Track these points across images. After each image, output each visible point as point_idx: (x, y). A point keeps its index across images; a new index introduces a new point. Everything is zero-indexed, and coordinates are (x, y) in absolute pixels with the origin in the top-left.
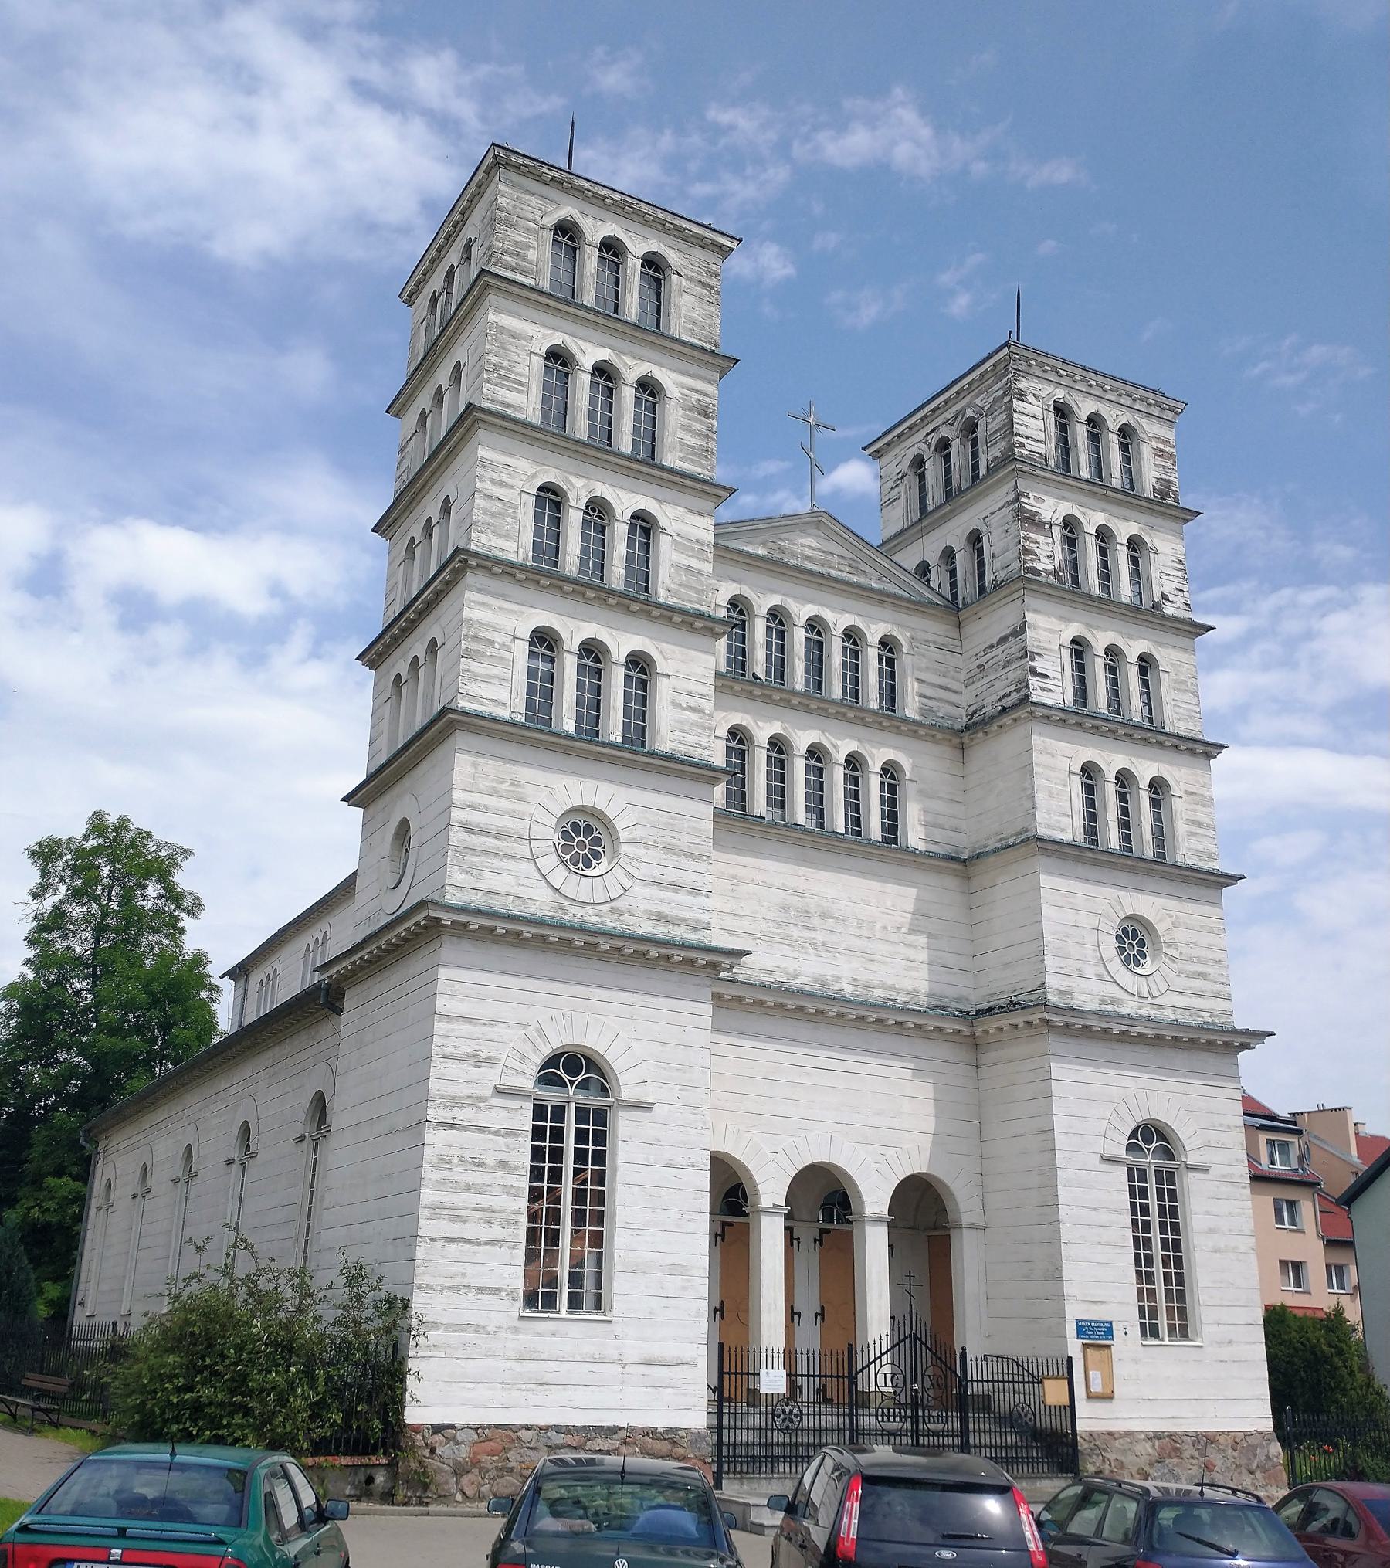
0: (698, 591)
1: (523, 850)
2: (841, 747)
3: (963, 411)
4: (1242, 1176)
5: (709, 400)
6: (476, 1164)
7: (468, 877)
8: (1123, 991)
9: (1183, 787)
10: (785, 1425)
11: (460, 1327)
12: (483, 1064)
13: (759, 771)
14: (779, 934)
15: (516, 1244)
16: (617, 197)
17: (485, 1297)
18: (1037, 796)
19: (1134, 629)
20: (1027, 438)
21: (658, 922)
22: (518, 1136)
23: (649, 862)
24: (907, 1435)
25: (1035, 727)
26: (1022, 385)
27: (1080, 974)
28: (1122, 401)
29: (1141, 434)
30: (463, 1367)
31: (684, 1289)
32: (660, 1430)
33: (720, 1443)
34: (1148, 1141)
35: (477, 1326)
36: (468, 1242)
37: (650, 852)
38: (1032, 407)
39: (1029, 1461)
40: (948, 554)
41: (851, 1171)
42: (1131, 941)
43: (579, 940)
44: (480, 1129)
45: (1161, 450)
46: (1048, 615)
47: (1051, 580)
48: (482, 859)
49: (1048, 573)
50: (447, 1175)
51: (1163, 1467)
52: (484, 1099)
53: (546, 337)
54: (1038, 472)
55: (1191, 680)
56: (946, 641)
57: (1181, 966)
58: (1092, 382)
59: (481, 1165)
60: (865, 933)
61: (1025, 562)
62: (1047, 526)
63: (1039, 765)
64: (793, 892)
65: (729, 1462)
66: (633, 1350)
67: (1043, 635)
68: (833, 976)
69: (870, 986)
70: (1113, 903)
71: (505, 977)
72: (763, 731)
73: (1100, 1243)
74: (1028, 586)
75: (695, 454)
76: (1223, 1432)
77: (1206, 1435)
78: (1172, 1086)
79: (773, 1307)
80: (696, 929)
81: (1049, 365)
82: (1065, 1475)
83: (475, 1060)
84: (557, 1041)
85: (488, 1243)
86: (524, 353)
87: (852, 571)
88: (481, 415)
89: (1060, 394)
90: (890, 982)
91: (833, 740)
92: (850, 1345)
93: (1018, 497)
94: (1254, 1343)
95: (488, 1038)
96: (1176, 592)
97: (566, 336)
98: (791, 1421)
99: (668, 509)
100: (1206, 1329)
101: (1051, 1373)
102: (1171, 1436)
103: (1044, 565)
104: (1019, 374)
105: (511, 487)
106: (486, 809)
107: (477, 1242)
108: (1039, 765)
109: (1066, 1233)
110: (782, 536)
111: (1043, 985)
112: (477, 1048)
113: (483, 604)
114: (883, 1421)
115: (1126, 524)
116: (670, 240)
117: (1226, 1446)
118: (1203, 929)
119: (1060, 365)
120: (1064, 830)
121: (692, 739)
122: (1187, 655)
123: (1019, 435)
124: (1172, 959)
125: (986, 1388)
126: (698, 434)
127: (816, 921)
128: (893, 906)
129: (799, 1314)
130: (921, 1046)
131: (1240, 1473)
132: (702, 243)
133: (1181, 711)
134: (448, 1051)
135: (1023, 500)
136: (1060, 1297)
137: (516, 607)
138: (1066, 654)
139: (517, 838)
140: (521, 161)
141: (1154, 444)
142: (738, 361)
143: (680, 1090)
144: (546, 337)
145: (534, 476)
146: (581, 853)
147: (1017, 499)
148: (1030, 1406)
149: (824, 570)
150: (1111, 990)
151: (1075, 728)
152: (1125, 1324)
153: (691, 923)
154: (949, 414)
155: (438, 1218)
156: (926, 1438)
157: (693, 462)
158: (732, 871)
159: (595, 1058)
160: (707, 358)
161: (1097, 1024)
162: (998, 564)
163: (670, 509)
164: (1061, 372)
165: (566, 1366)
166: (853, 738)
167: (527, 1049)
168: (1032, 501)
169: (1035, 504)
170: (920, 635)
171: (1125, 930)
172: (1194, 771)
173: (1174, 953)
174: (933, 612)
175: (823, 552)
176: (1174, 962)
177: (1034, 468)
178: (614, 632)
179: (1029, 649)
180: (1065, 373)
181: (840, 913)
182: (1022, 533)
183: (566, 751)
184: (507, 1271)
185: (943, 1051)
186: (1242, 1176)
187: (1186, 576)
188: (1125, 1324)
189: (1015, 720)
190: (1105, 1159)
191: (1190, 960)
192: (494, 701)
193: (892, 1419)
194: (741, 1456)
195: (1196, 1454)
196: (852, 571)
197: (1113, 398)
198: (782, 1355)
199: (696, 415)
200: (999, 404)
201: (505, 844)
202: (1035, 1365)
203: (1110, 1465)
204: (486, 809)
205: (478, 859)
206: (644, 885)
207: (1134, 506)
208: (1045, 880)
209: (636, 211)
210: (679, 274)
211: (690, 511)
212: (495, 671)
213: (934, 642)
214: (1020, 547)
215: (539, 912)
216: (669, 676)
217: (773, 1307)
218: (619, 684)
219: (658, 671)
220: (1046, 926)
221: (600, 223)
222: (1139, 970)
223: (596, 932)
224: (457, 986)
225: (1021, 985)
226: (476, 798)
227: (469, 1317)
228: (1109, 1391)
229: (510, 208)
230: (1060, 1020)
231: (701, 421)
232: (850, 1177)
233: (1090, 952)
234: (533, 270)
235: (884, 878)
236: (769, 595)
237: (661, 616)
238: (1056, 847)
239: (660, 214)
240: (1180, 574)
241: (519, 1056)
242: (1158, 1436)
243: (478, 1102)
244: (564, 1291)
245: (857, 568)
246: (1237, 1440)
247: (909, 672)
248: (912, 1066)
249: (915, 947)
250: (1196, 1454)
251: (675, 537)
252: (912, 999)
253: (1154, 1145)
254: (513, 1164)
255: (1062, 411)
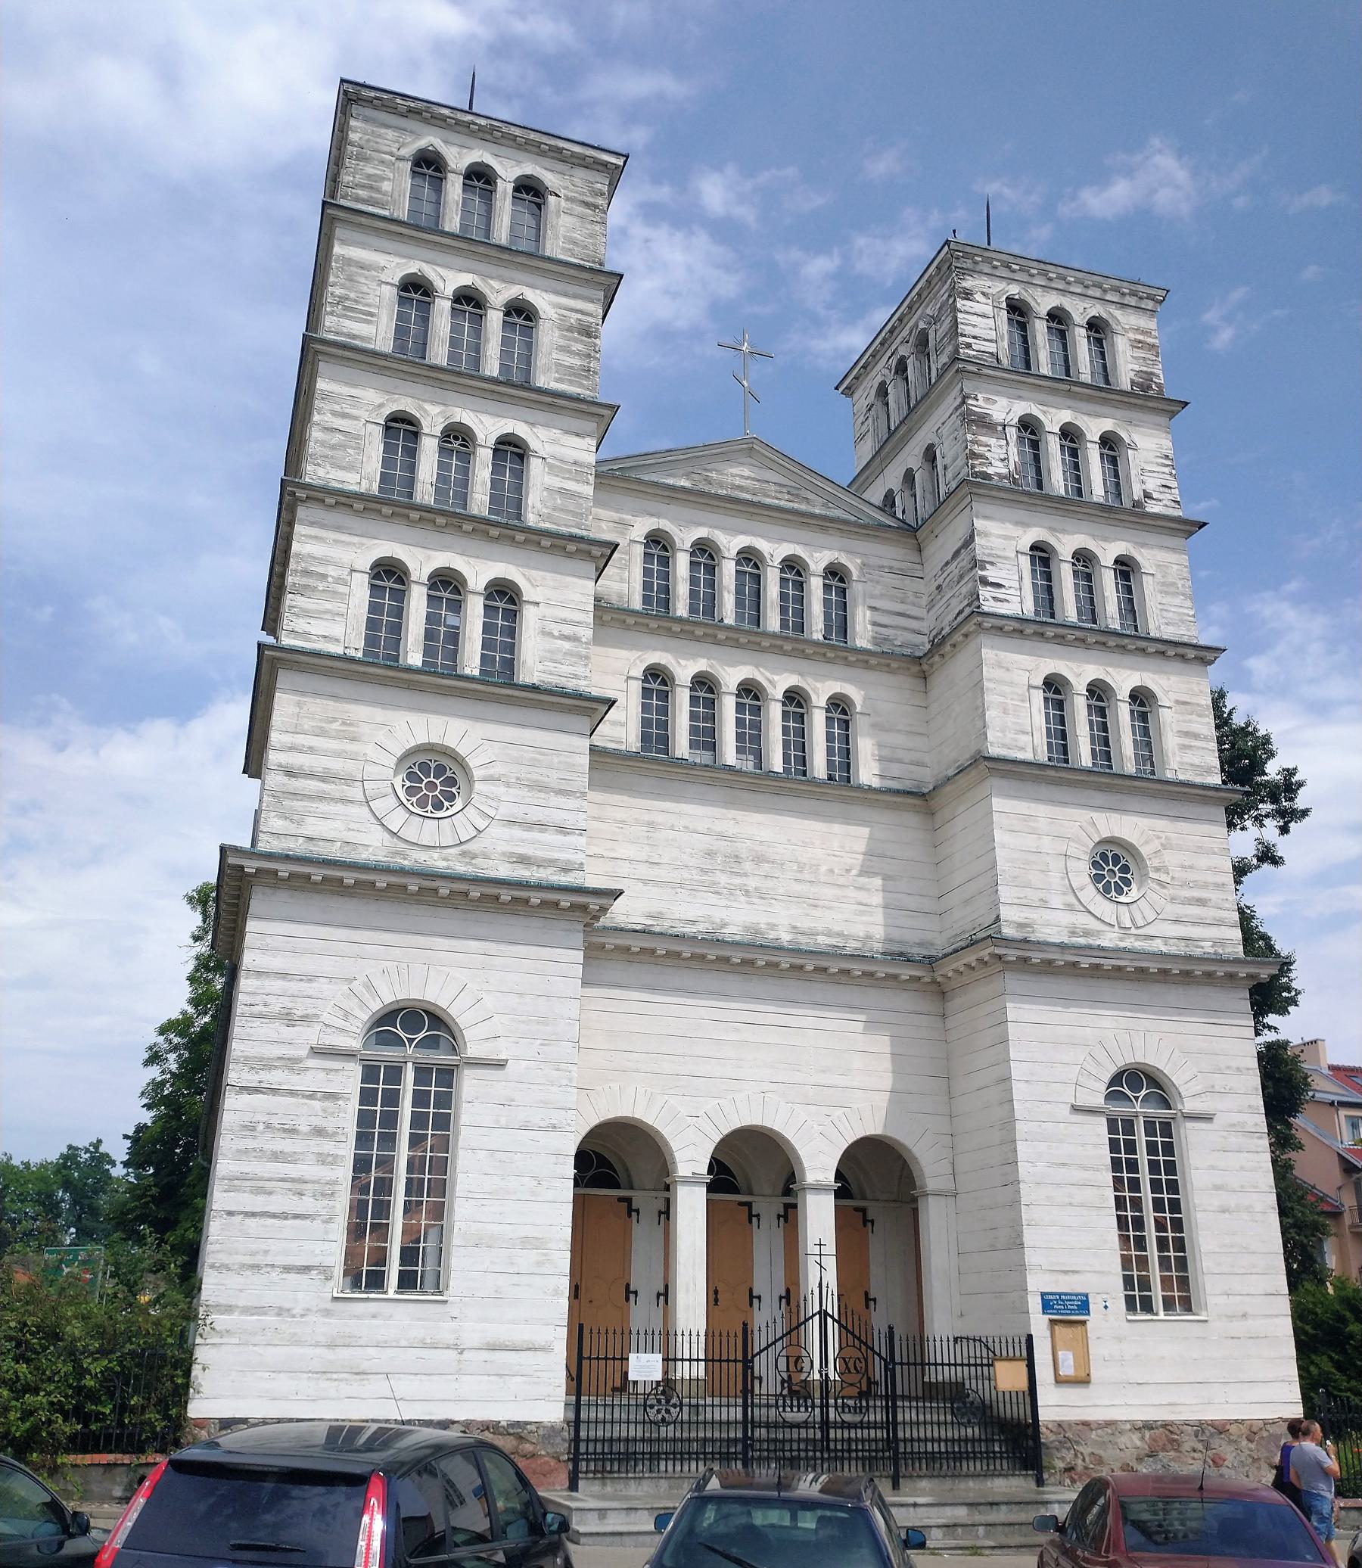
0: (575, 514)
1: (356, 792)
2: (778, 682)
3: (916, 325)
4: (1256, 1124)
5: (590, 319)
6: (285, 1131)
7: (287, 823)
8: (1099, 922)
9: (1173, 696)
10: (660, 1417)
11: (259, 1310)
12: (298, 1023)
13: (681, 711)
14: (704, 881)
15: (330, 1219)
16: (482, 122)
17: (292, 1277)
18: (987, 713)
19: (1109, 530)
20: (975, 337)
21: (521, 865)
22: (338, 1099)
23: (509, 801)
24: (814, 1428)
25: (984, 639)
26: (968, 283)
27: (1043, 905)
28: (1090, 292)
29: (1114, 326)
30: (261, 1355)
31: (539, 1263)
32: (502, 1423)
33: (577, 1439)
34: (1136, 1088)
35: (280, 1308)
36: (274, 1216)
37: (511, 790)
38: (982, 306)
39: (989, 1456)
40: (909, 477)
41: (788, 1135)
42: (1111, 867)
43: (785, 962)
44: (292, 1093)
45: (1140, 342)
46: (1002, 521)
47: (1006, 482)
48: (306, 804)
49: (1001, 476)
50: (250, 1144)
51: (1155, 1463)
52: (297, 1060)
53: (397, 265)
54: (985, 371)
55: (1182, 582)
56: (903, 566)
57: (1172, 891)
58: (1051, 275)
59: (293, 1132)
60: (807, 877)
61: (973, 467)
62: (1000, 428)
63: (989, 680)
64: (721, 836)
65: (588, 1460)
66: (473, 1333)
67: (996, 543)
68: (768, 924)
69: (813, 934)
70: (1085, 824)
71: (328, 929)
72: (684, 670)
73: (1071, 1204)
74: (975, 490)
75: (574, 375)
76: (1236, 1421)
77: (1212, 1424)
78: (1166, 1026)
79: (692, 1286)
80: (566, 870)
81: (998, 260)
82: (1024, 1472)
83: (288, 1018)
84: (389, 995)
85: (296, 1217)
86: (375, 284)
87: (792, 498)
88: (318, 347)
89: (1014, 290)
90: (837, 928)
91: (767, 674)
92: (745, 1324)
93: (965, 398)
94: (1277, 1316)
95: (305, 994)
96: (1162, 489)
97: (424, 264)
98: (668, 1411)
99: (542, 432)
100: (1211, 1301)
101: (1004, 1353)
102: (1166, 1425)
103: (996, 468)
104: (964, 272)
105: (355, 418)
106: (311, 750)
107: (284, 1216)
108: (989, 680)
109: (1027, 1193)
110: (709, 467)
111: (998, 919)
112: (290, 1005)
113: (316, 537)
114: (784, 1410)
115: (1098, 420)
116: (547, 162)
117: (1240, 1436)
118: (1200, 850)
119: (1011, 259)
120: (1022, 749)
121: (565, 669)
122: (1177, 556)
123: (965, 336)
124: (1162, 884)
125: (959, 1374)
126: (578, 354)
127: (748, 866)
128: (841, 847)
129: (759, 1298)
130: (874, 996)
131: (1259, 1468)
132: (584, 163)
133: (1170, 615)
134: (255, 1009)
135: (970, 402)
136: (1021, 1268)
137: (355, 539)
138: (1025, 562)
139: (348, 780)
140: (372, 94)
141: (1132, 335)
142: (1187, 404)
143: (542, 1045)
144: (397, 265)
145: (381, 406)
146: (437, 793)
147: (963, 402)
148: (977, 1392)
149: (756, 499)
150: (1084, 921)
151: (1035, 638)
152: (1105, 1296)
153: (559, 864)
154: (905, 333)
155: (237, 1190)
156: (908, 1435)
157: (571, 382)
158: (647, 817)
159: (439, 1013)
160: (586, 276)
161: (1060, 958)
162: (949, 475)
163: (544, 431)
164: (1014, 266)
165: (390, 1352)
166: (792, 672)
167: (352, 1005)
168: (980, 403)
169: (984, 405)
170: (874, 561)
171: (1104, 856)
172: (1186, 679)
173: (1163, 877)
174: (887, 535)
175: (758, 481)
176: (1164, 887)
177: (986, 370)
178: (472, 560)
179: (978, 558)
180: (1018, 267)
181: (778, 857)
182: (969, 437)
183: (410, 686)
184: (318, 1247)
185: (904, 1000)
186: (1256, 1124)
187: (1174, 472)
188: (1105, 1296)
189: (966, 636)
190: (1076, 1109)
191: (1185, 884)
192: (325, 637)
193: (795, 1409)
194: (919, 1453)
195: (1200, 1446)
196: (792, 498)
197: (1079, 290)
198: (702, 1339)
199: (576, 335)
200: (944, 309)
201: (333, 786)
202: (1004, 1345)
203: (1084, 1460)
204: (311, 750)
205: (300, 803)
206: (504, 826)
207: (1106, 402)
208: (998, 803)
209: (505, 135)
210: (557, 195)
211: (567, 432)
212: (328, 606)
213: (891, 568)
214: (967, 451)
215: (372, 858)
216: (537, 604)
217: (692, 1286)
218: (476, 614)
219: (524, 599)
220: (1000, 854)
221: (465, 151)
222: (1122, 899)
223: (432, 876)
224: (269, 939)
225: (980, 921)
226: (300, 740)
227: (270, 1298)
228: (1082, 1374)
229: (363, 143)
230: (1012, 954)
231: (582, 341)
232: (787, 1142)
233: (1055, 879)
234: (387, 202)
235: (830, 818)
236: (693, 528)
237: (837, 657)
238: (1009, 767)
239: (532, 136)
240: (1167, 470)
241: (342, 1012)
242: (1148, 1426)
243: (291, 1064)
244: (393, 1270)
245: (798, 496)
246: (1255, 1429)
247: (860, 600)
248: (863, 1017)
249: (868, 890)
250: (1200, 1446)
251: (548, 460)
252: (863, 946)
253: (1143, 1092)
254: (330, 1130)
255: (1018, 310)
